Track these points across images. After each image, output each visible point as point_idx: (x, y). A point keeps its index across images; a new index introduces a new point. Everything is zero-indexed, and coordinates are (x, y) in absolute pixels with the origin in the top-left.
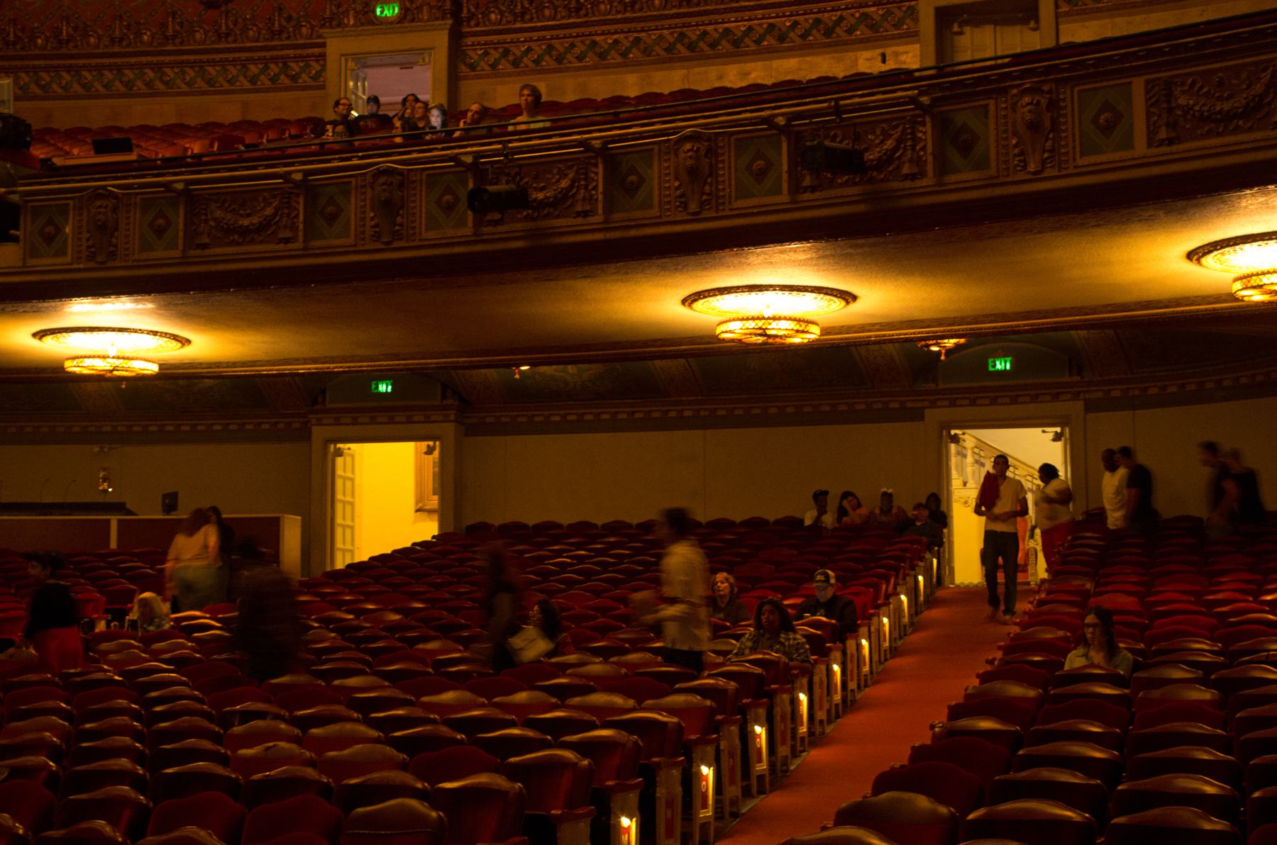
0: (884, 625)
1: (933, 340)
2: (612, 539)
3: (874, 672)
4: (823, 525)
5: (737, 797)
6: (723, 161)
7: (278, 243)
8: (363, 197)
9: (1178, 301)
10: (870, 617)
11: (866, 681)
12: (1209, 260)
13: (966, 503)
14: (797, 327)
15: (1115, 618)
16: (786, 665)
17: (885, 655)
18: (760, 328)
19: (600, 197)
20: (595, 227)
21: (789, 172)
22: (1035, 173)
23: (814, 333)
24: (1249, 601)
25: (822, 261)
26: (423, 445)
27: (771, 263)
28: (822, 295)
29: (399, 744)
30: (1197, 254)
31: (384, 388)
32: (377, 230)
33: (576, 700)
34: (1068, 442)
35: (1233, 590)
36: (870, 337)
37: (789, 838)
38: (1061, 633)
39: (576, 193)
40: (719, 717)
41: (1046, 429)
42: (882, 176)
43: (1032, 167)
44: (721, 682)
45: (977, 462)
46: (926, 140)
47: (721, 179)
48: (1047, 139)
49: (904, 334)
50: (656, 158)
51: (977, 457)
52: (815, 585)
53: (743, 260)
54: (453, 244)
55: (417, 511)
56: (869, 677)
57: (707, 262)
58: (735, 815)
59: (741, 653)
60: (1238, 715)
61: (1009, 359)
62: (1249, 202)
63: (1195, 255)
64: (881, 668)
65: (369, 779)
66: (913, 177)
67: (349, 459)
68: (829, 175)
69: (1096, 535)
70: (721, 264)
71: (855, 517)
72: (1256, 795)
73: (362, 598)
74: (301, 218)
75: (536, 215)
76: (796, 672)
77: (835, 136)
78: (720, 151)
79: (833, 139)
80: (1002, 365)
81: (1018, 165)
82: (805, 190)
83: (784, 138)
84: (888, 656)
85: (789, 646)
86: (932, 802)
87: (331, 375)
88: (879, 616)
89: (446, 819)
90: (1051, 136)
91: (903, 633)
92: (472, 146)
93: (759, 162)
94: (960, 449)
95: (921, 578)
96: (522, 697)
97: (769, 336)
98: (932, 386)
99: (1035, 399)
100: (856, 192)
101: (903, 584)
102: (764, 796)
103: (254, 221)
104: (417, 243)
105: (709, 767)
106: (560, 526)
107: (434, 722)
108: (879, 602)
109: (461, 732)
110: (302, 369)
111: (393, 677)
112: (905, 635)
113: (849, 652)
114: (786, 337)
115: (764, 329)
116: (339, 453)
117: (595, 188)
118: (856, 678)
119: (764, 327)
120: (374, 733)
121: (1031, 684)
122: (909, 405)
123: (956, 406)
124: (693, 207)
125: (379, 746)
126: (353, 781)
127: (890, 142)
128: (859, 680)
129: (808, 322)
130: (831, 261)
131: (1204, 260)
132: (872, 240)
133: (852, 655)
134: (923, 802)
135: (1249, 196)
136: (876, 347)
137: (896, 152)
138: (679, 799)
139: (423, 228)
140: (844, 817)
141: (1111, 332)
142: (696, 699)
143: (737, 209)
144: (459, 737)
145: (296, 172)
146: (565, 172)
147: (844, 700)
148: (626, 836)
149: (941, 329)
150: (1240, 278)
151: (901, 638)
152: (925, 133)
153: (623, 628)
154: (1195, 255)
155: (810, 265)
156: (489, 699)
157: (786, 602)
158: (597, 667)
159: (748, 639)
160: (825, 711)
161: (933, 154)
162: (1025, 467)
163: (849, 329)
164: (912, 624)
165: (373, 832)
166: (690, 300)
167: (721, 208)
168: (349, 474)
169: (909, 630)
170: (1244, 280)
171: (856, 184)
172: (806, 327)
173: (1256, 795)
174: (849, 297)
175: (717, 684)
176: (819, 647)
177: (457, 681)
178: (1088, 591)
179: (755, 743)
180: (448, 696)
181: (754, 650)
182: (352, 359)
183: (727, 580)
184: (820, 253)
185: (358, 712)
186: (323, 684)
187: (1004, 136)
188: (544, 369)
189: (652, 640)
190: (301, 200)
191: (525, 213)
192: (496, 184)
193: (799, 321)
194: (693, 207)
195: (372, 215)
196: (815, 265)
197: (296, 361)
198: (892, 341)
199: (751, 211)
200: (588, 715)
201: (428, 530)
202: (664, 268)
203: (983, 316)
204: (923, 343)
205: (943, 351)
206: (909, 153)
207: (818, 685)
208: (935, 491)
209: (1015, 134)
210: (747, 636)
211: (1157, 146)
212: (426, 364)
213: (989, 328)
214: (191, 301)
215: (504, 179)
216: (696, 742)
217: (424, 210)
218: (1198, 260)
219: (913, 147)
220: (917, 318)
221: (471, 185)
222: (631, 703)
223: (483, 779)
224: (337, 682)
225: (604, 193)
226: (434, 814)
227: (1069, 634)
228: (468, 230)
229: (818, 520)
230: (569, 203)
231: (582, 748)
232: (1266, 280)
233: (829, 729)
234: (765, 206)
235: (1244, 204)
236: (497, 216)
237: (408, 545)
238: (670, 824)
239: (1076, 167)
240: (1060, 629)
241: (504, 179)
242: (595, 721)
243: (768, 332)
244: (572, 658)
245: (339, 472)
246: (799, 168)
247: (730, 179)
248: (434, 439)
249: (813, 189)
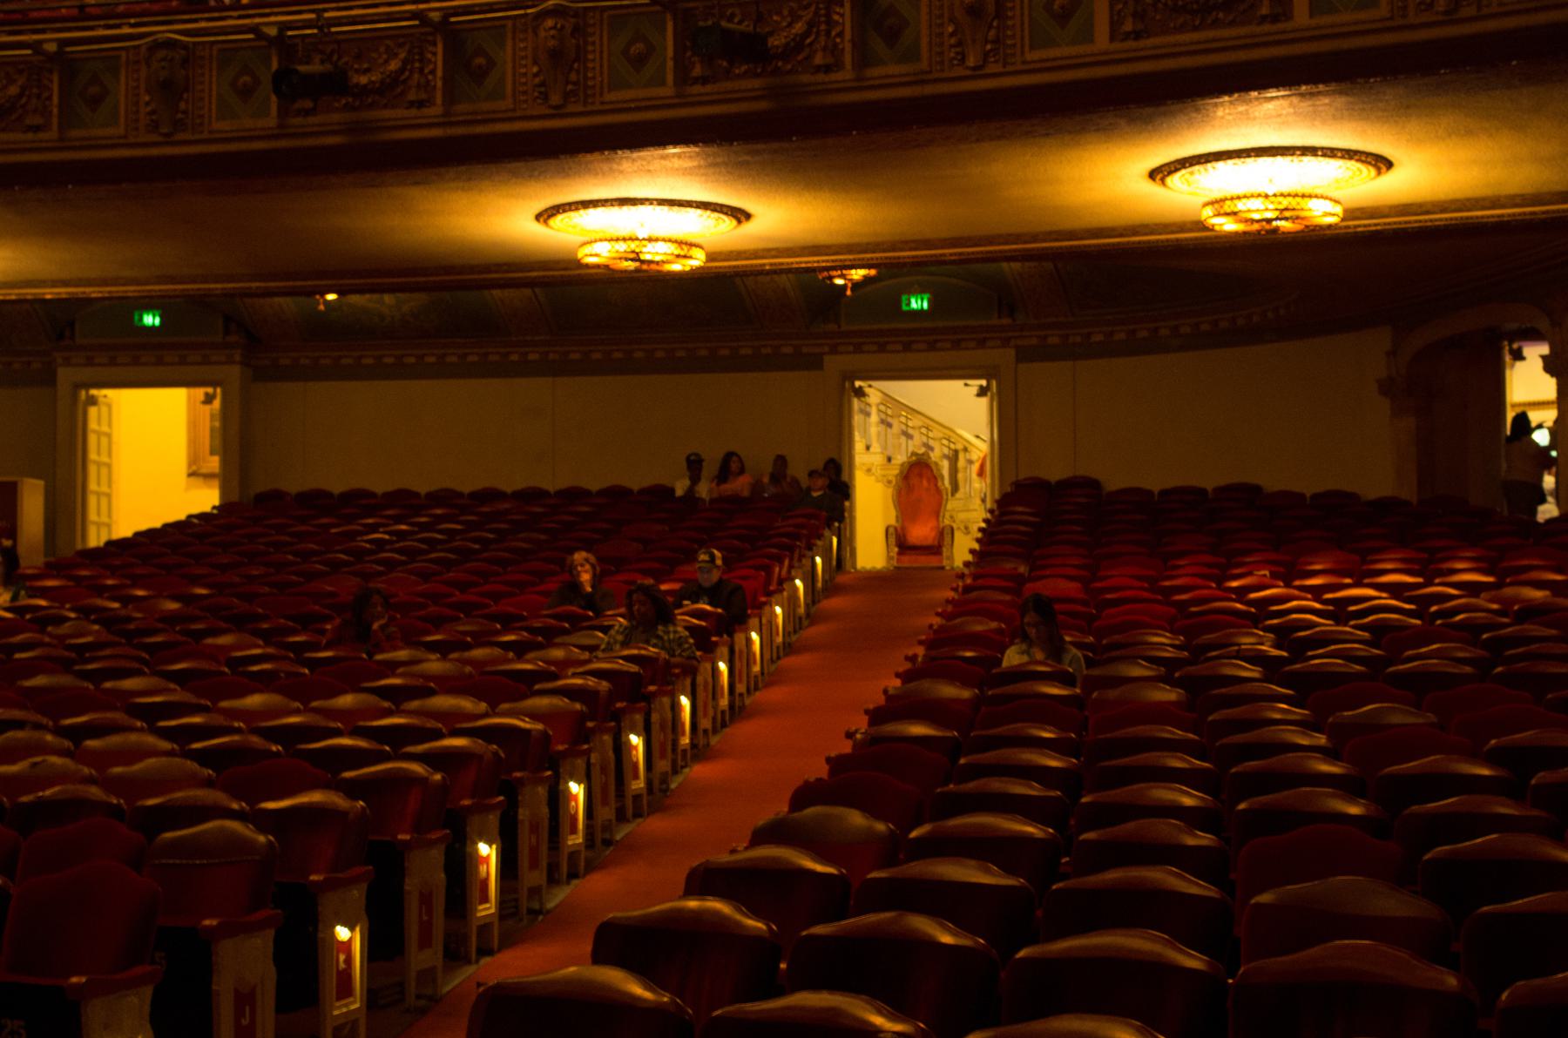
0: (776, 615)
1: (836, 270)
2: (439, 512)
3: (766, 671)
4: (697, 495)
5: (610, 820)
6: (593, 43)
7: (25, 132)
8: (135, 76)
9: (1135, 230)
10: (760, 606)
11: (756, 684)
12: (1175, 180)
13: (869, 470)
14: (677, 251)
15: (1057, 607)
16: (667, 662)
17: (778, 652)
18: (633, 252)
19: (439, 84)
20: (431, 120)
21: (675, 59)
22: (974, 69)
23: (698, 260)
24: (1211, 588)
25: (711, 170)
26: (200, 393)
27: (649, 171)
28: (708, 212)
29: (203, 757)
30: (1162, 172)
31: (150, 320)
32: (154, 117)
33: (415, 704)
34: (996, 398)
35: (1187, 575)
36: (764, 265)
37: (704, 860)
38: (994, 625)
39: (408, 78)
40: (590, 724)
41: (969, 382)
42: (789, 67)
43: (971, 62)
44: (591, 682)
45: (883, 421)
46: (843, 24)
47: (590, 65)
48: (990, 27)
49: (806, 263)
50: (510, 35)
51: (883, 416)
52: (698, 565)
53: (615, 166)
54: (252, 139)
55: (191, 475)
56: (760, 679)
57: (570, 168)
58: (608, 843)
59: (609, 648)
60: (1210, 718)
61: (926, 297)
62: (1227, 111)
63: (1158, 174)
64: (773, 668)
65: (170, 801)
66: (827, 69)
67: (104, 409)
68: (725, 64)
69: (1027, 510)
70: (588, 171)
71: (740, 485)
72: (1242, 806)
73: (129, 582)
74: (55, 99)
75: (357, 103)
76: (677, 671)
77: (733, 15)
78: (590, 30)
79: (730, 20)
80: (918, 303)
81: (954, 59)
82: (696, 81)
83: (669, 16)
84: (781, 654)
85: (669, 640)
86: (867, 818)
87: (88, 301)
88: (771, 606)
89: (277, 845)
90: (995, 24)
91: (797, 627)
92: (276, 14)
93: (638, 45)
94: (863, 406)
95: (818, 560)
96: (346, 700)
97: (643, 262)
98: (832, 327)
99: (956, 345)
100: (756, 86)
101: (799, 567)
102: (640, 820)
103: (373, 79)
104: (205, 135)
105: (579, 784)
106: (372, 495)
107: (238, 731)
108: (772, 588)
109: (276, 742)
110: (49, 293)
111: (181, 678)
112: (801, 628)
113: (737, 649)
114: (663, 262)
115: (637, 253)
116: (93, 401)
117: (433, 72)
118: (745, 678)
119: (637, 250)
120: (166, 745)
121: (965, 683)
122: (805, 350)
123: (862, 352)
124: (555, 99)
125: (177, 760)
126: (151, 802)
127: (800, 24)
128: (748, 682)
129: (691, 245)
130: (723, 170)
131: (1169, 180)
132: (775, 145)
133: (741, 652)
134: (856, 819)
135: (1228, 104)
136: (768, 278)
137: (807, 37)
138: (546, 823)
139: (214, 116)
140: (761, 836)
141: (1049, 265)
142: (561, 702)
143: (611, 103)
144: (274, 749)
145: (50, 40)
146: (395, 51)
147: (731, 706)
148: (485, 867)
149: (851, 257)
150: (1212, 203)
151: (795, 632)
152: (842, 15)
153: (459, 618)
154: (1158, 174)
155: (697, 174)
156: (305, 703)
157: (664, 587)
158: (434, 665)
159: (618, 632)
160: (711, 719)
161: (852, 41)
162: (940, 428)
163: (739, 255)
164: (808, 615)
165: (184, 862)
166: (545, 216)
167: (590, 101)
168: (105, 428)
169: (806, 623)
170: (1216, 206)
171: (757, 75)
172: (688, 250)
173: (1242, 806)
174: (740, 215)
175: (588, 685)
176: (705, 642)
177: (263, 682)
178: (1021, 575)
179: (631, 756)
180: (254, 700)
181: (625, 645)
182: (115, 281)
183: (587, 560)
184: (710, 160)
185: (142, 720)
186: (91, 687)
187: (938, 21)
188: (354, 299)
189: (499, 633)
190: (55, 78)
191: (344, 102)
192: (307, 63)
193: (680, 243)
194: (555, 99)
195: (147, 98)
196: (703, 175)
197: (41, 283)
198: (789, 271)
199: (625, 105)
200: (433, 722)
201: (206, 499)
202: (516, 174)
203: (902, 242)
204: (826, 274)
205: (850, 285)
206: (822, 39)
207: (702, 687)
208: (834, 455)
209: (952, 20)
210: (616, 628)
211: (1123, 40)
212: (209, 289)
213: (908, 257)
214: (1291, 110)
215: (317, 58)
216: (564, 755)
217: (214, 93)
218: (1163, 180)
219: (828, 33)
220: (822, 243)
221: (275, 65)
222: (483, 706)
223: (316, 797)
224: (108, 685)
225: (444, 79)
226: (262, 839)
227: (1003, 626)
228: (271, 121)
229: (690, 492)
230: (399, 90)
231: (433, 760)
232: (1240, 206)
233: (714, 740)
234: (656, 99)
235: (1220, 113)
236: (308, 104)
237: (182, 517)
238: (534, 851)
239: (1024, 62)
240: (993, 620)
241: (317, 58)
242: (441, 729)
243: (643, 257)
244: (403, 654)
245: (93, 425)
246: (689, 54)
247: (601, 66)
248: (213, 384)
249: (704, 80)
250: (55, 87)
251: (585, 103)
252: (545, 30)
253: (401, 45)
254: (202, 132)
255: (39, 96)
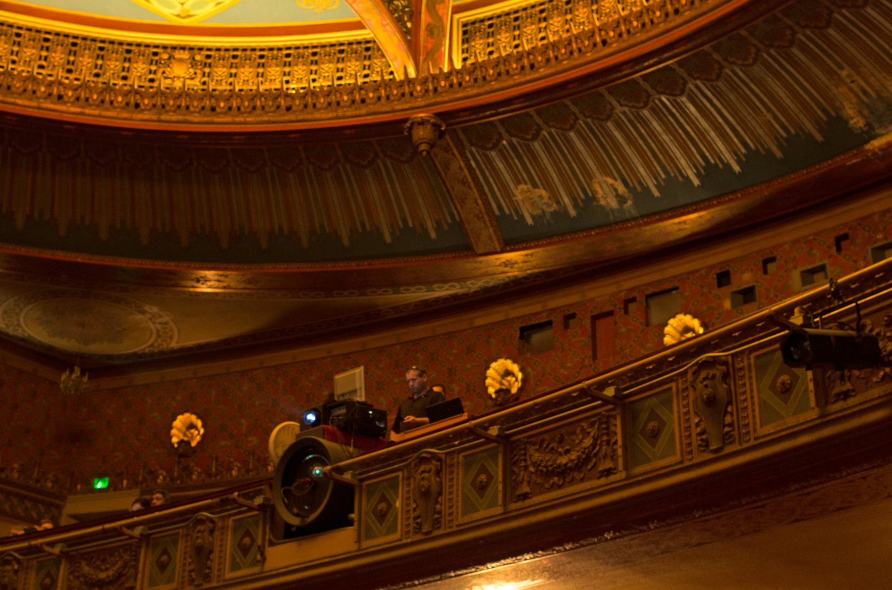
7: (599, 478)
8: (685, 402)
32: (704, 437)
39: (598, 452)
104: (753, 442)
191: (881, 374)
217: (756, 400)
250: (619, 430)
251: (740, 444)
252: (701, 383)
253: (592, 425)
254: (748, 441)
255: (608, 442)
